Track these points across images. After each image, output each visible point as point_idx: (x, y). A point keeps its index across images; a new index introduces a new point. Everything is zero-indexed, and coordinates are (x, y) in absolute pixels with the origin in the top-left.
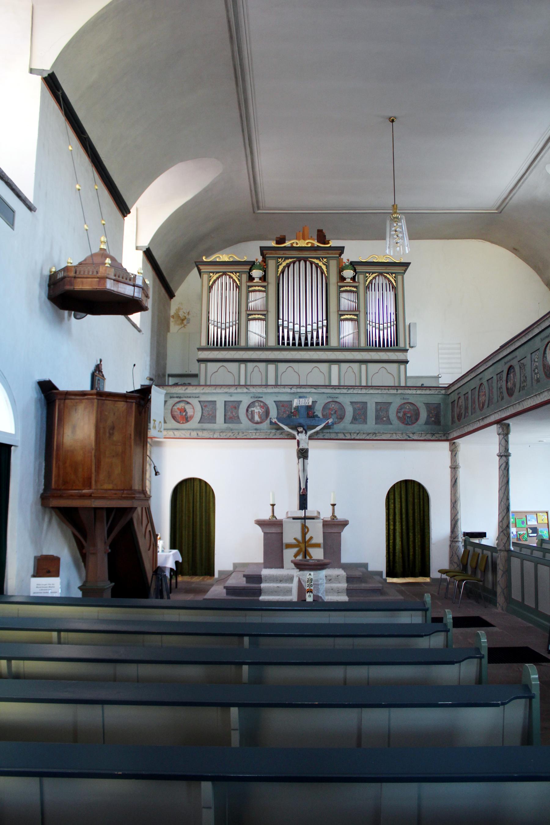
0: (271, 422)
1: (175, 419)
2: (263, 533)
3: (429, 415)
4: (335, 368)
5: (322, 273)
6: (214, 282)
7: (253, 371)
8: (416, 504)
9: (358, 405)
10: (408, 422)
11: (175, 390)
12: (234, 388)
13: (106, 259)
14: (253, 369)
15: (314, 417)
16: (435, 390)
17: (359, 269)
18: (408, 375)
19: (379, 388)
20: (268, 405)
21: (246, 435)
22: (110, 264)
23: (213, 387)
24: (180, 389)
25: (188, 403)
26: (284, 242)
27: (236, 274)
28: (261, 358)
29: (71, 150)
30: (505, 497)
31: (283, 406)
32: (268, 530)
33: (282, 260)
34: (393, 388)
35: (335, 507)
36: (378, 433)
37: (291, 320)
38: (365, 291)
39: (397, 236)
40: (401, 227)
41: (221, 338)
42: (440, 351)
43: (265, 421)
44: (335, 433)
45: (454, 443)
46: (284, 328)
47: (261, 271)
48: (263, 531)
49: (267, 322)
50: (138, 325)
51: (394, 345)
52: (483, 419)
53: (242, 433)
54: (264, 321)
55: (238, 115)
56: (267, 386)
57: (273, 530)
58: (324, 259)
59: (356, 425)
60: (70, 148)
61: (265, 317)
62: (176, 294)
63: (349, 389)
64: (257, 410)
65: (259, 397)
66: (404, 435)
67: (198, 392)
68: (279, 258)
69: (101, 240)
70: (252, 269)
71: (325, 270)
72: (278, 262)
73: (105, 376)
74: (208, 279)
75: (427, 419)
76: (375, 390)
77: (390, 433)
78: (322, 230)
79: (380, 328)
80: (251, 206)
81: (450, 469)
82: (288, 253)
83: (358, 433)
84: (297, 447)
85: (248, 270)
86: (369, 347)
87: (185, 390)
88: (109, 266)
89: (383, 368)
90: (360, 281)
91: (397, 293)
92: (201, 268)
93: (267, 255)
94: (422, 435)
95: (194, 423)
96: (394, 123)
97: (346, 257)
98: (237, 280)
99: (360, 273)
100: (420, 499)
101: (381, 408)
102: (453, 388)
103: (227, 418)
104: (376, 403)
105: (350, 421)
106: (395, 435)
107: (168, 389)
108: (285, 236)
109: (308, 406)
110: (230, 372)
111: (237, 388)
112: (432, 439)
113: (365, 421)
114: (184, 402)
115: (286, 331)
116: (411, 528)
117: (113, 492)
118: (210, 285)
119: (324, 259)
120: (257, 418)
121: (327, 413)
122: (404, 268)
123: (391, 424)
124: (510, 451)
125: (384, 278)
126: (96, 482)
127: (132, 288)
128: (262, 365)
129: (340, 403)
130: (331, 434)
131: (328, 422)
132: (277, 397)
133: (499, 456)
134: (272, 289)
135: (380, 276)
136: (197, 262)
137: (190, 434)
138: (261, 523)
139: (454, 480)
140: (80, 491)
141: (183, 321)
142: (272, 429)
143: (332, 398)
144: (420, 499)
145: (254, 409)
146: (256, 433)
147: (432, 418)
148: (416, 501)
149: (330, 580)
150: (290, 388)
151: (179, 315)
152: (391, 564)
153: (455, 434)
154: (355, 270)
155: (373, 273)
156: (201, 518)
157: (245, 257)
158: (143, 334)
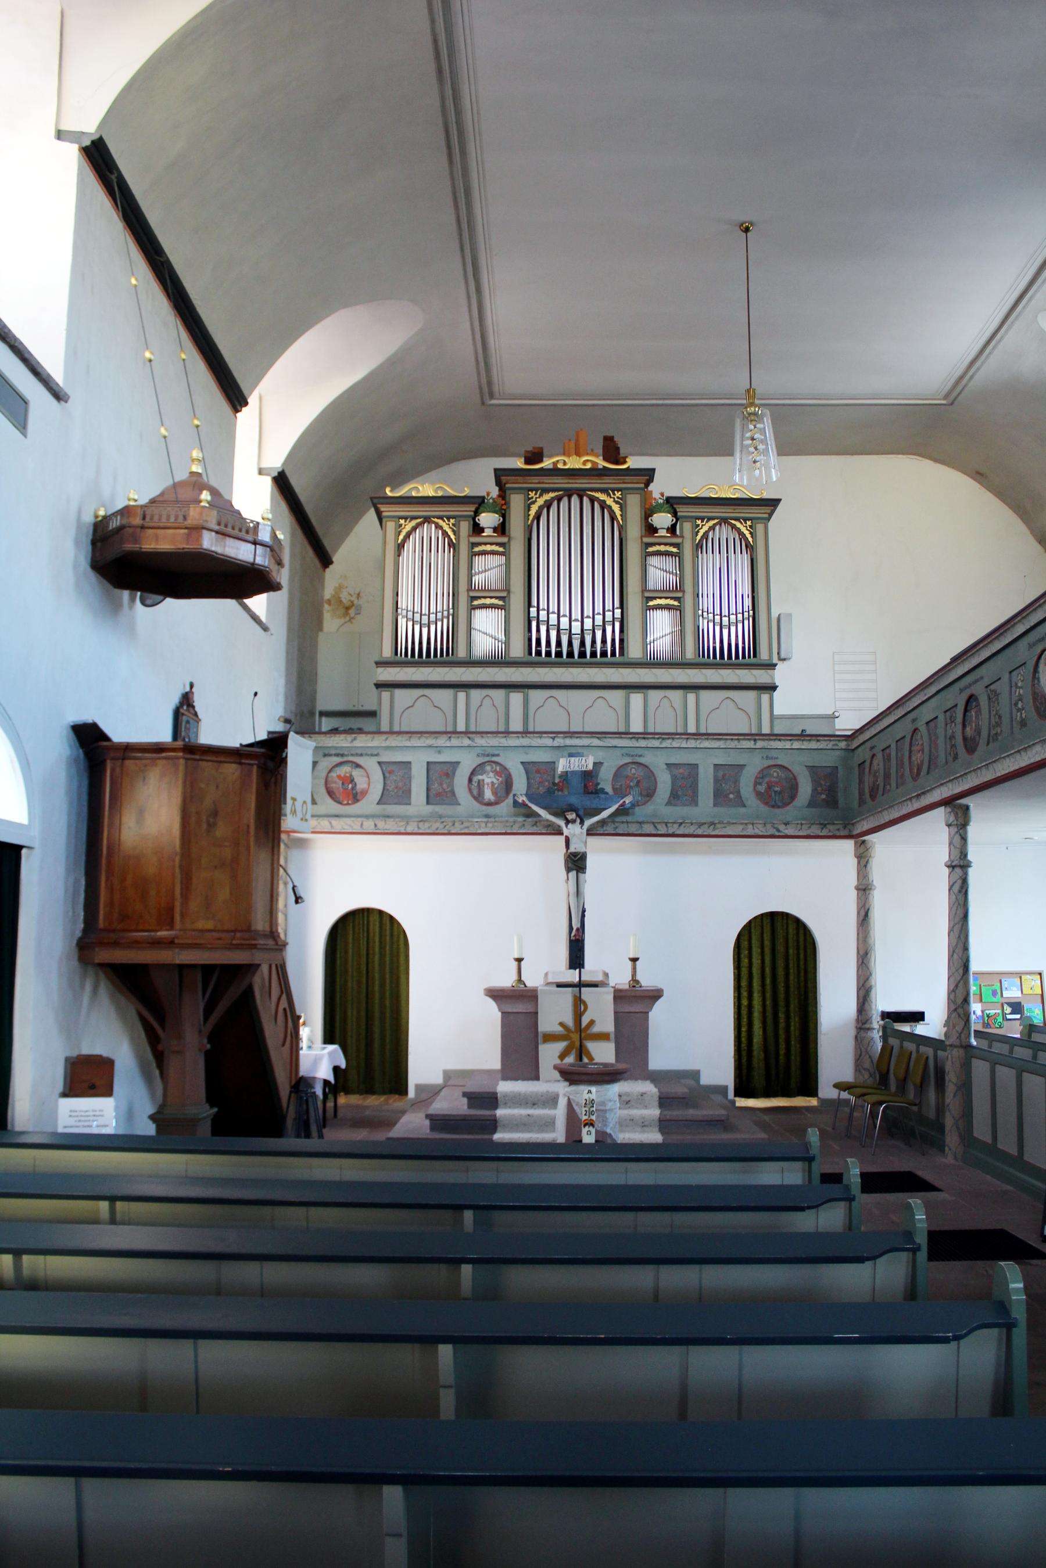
0: (515, 803)
1: (333, 796)
2: (500, 1014)
3: (816, 789)
4: (637, 699)
5: (613, 518)
6: (408, 536)
7: (481, 705)
8: (791, 958)
9: (681, 771)
10: (775, 802)
11: (333, 740)
12: (444, 738)
13: (201, 493)
14: (482, 701)
15: (597, 792)
16: (828, 742)
17: (682, 511)
18: (776, 713)
19: (721, 737)
20: (510, 770)
21: (468, 827)
22: (208, 503)
23: (404, 735)
24: (342, 740)
25: (358, 766)
26: (541, 461)
27: (449, 521)
28: (496, 680)
29: (136, 286)
30: (961, 945)
31: (538, 772)
32: (510, 1008)
33: (536, 494)
34: (747, 737)
35: (638, 963)
36: (719, 823)
37: (553, 607)
38: (695, 552)
39: (756, 448)
40: (763, 431)
41: (421, 643)
42: (837, 668)
43: (504, 801)
44: (638, 822)
45: (864, 842)
46: (541, 623)
47: (497, 515)
48: (499, 1010)
49: (507, 612)
50: (263, 619)
51: (749, 656)
52: (918, 796)
53: (460, 823)
54: (502, 610)
55: (453, 218)
56: (507, 733)
57: (520, 1007)
58: (616, 492)
59: (678, 809)
60: (134, 281)
61: (504, 602)
62: (334, 559)
63: (663, 739)
64: (489, 779)
65: (493, 755)
66: (769, 826)
67: (376, 745)
68: (531, 490)
69: (191, 457)
70: (480, 511)
71: (618, 512)
72: (529, 499)
73: (200, 716)
74: (395, 530)
75: (812, 796)
76: (714, 741)
77: (742, 824)
78: (613, 437)
79: (723, 624)
80: (478, 391)
81: (856, 892)
82: (547, 481)
83: (681, 824)
84: (565, 850)
85: (472, 513)
86: (701, 660)
87: (352, 741)
88: (207, 505)
89: (729, 700)
90: (684, 535)
91: (754, 557)
92: (382, 509)
93: (507, 486)
94: (803, 826)
95: (369, 804)
96: (748, 234)
97: (659, 489)
98: (450, 533)
99: (684, 520)
100: (798, 949)
101: (724, 776)
102: (862, 738)
103: (431, 794)
104: (715, 765)
105: (666, 801)
106: (750, 826)
107: (319, 739)
108: (542, 448)
109: (585, 771)
110: (438, 708)
111: (450, 737)
112: (821, 834)
113: (694, 801)
114: (350, 765)
115: (543, 629)
116: (781, 1003)
117: (215, 935)
118: (399, 541)
119: (616, 492)
120: (488, 795)
121: (621, 786)
122: (768, 510)
123: (744, 806)
124: (970, 857)
125: (730, 528)
126: (183, 916)
127: (252, 547)
128: (498, 694)
129: (646, 766)
130: (629, 825)
131: (624, 802)
132: (527, 754)
133: (948, 867)
134: (517, 549)
135: (723, 524)
136: (375, 498)
137: (362, 825)
138: (496, 995)
139: (863, 913)
140: (153, 934)
141: (347, 609)
142: (517, 815)
143: (632, 756)
144: (798, 949)
145: (484, 777)
146: (486, 822)
147: (821, 794)
148: (791, 951)
149: (627, 1103)
150: (551, 737)
151: (340, 598)
152: (744, 1071)
153: (866, 826)
154: (675, 514)
155: (710, 519)
156: (382, 985)
157: (466, 489)
158: (272, 634)
